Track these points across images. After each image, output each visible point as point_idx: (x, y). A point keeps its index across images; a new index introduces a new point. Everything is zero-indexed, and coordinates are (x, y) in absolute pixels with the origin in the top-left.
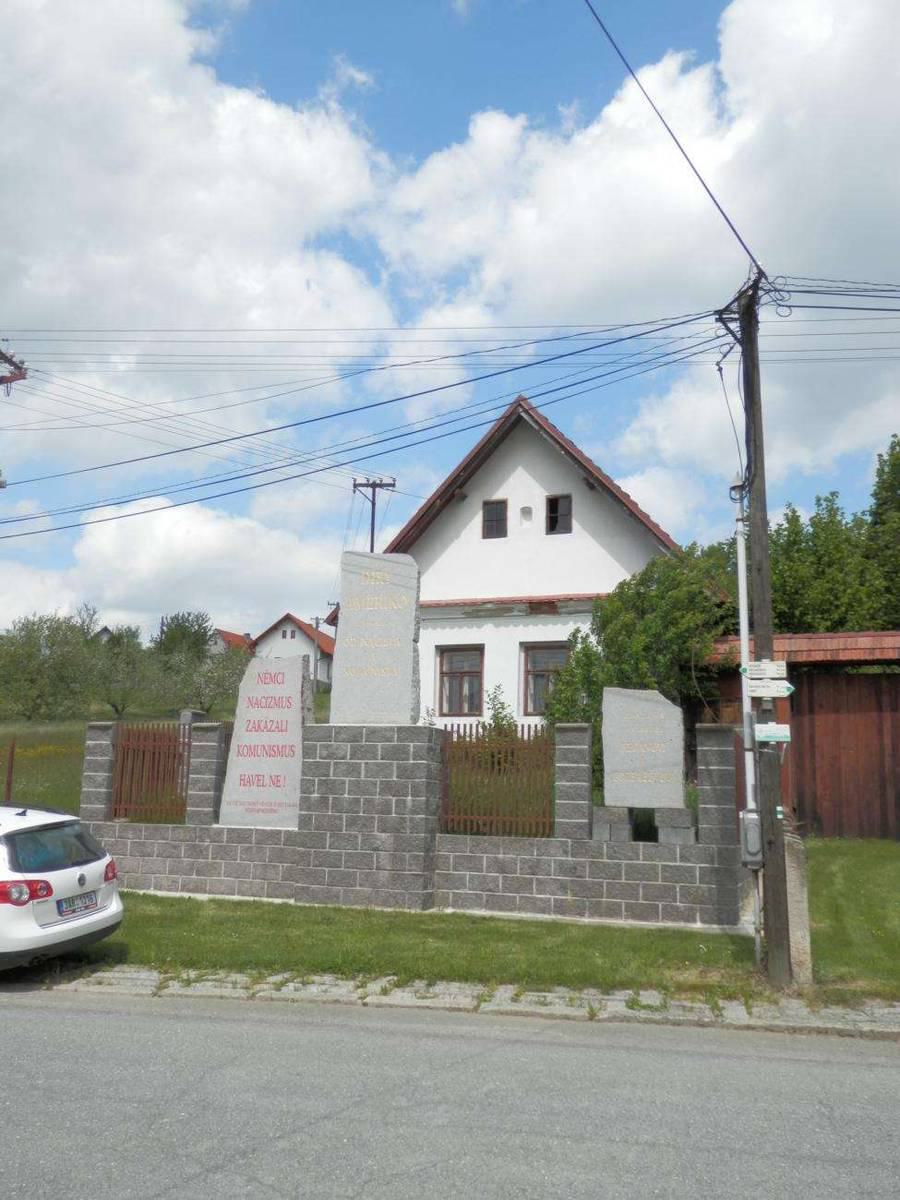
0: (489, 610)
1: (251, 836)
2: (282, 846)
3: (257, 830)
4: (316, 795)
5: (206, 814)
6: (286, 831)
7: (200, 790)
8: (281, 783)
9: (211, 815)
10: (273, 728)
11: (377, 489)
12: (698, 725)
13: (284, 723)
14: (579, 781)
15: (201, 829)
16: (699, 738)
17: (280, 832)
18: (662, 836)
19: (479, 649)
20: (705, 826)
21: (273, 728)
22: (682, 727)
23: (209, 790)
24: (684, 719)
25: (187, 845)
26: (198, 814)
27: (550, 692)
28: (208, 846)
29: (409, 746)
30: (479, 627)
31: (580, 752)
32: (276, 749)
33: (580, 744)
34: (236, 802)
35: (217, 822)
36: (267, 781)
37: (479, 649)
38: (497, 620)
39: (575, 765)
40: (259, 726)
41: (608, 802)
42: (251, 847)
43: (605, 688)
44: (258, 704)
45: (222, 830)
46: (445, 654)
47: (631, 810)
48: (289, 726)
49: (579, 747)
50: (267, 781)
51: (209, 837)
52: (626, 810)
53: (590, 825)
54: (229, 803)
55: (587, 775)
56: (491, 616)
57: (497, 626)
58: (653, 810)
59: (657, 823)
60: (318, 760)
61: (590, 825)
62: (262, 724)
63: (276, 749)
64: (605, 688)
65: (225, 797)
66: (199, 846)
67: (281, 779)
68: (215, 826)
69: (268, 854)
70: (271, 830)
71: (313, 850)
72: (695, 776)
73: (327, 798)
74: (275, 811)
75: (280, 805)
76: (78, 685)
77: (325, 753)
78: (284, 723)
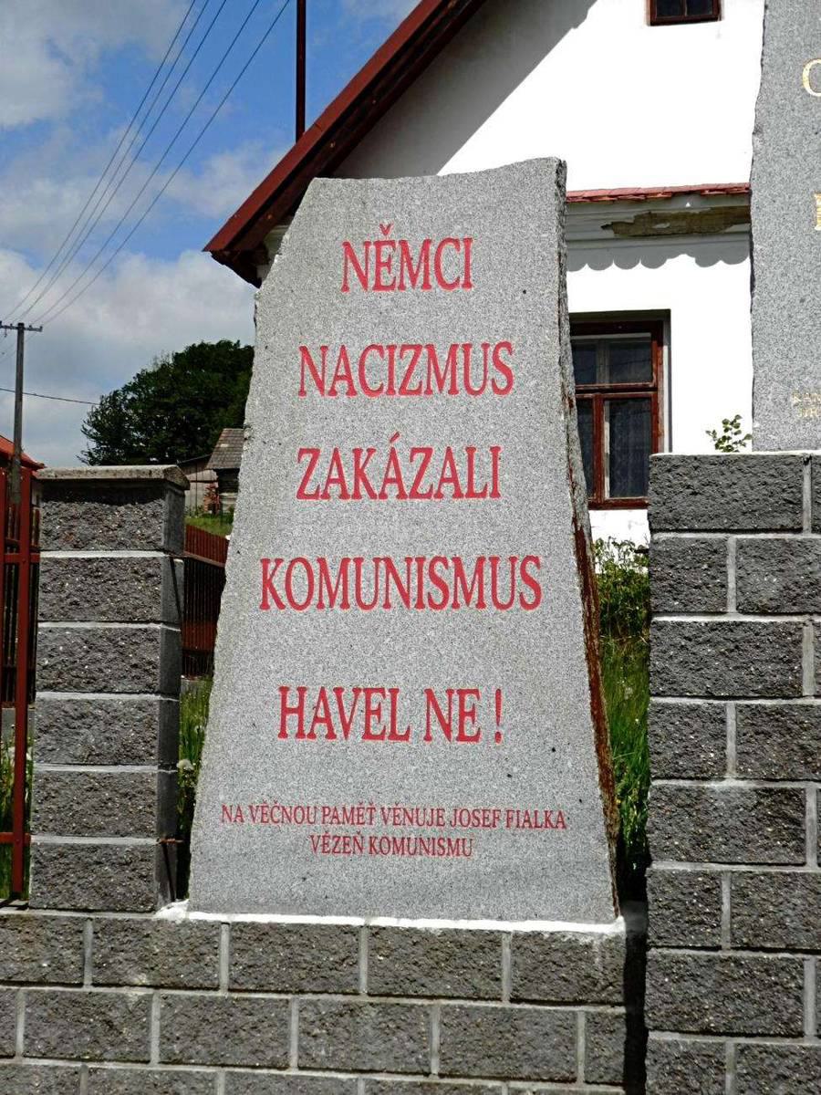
0: (685, 216)
1: (349, 960)
2: (506, 1004)
3: (377, 932)
4: (731, 782)
5: (126, 863)
6: (522, 942)
7: (92, 758)
8: (485, 719)
9: (151, 868)
10: (430, 480)
11: (16, 332)
13: (483, 457)
15: (104, 930)
17: (493, 940)
19: (654, 326)
21: (430, 480)
23: (137, 759)
25: (44, 1001)
26: (88, 860)
28: (145, 1004)
29: (717, 551)
30: (654, 263)
32: (448, 575)
34: (264, 812)
35: (179, 890)
36: (412, 714)
37: (654, 326)
38: (711, 244)
40: (359, 474)
42: (352, 1010)
44: (351, 379)
45: (208, 933)
46: (416, 388)
48: (505, 477)
50: (412, 714)
51: (145, 962)
54: (232, 814)
56: (689, 233)
57: (704, 261)
60: (732, 617)
62: (376, 469)
63: (448, 575)
65: (212, 794)
66: (101, 1008)
67: (485, 706)
68: (174, 912)
69: (436, 1040)
70: (445, 932)
71: (731, 1043)
73: (796, 798)
74: (455, 847)
75: (484, 820)
77: (769, 586)
78: (483, 457)
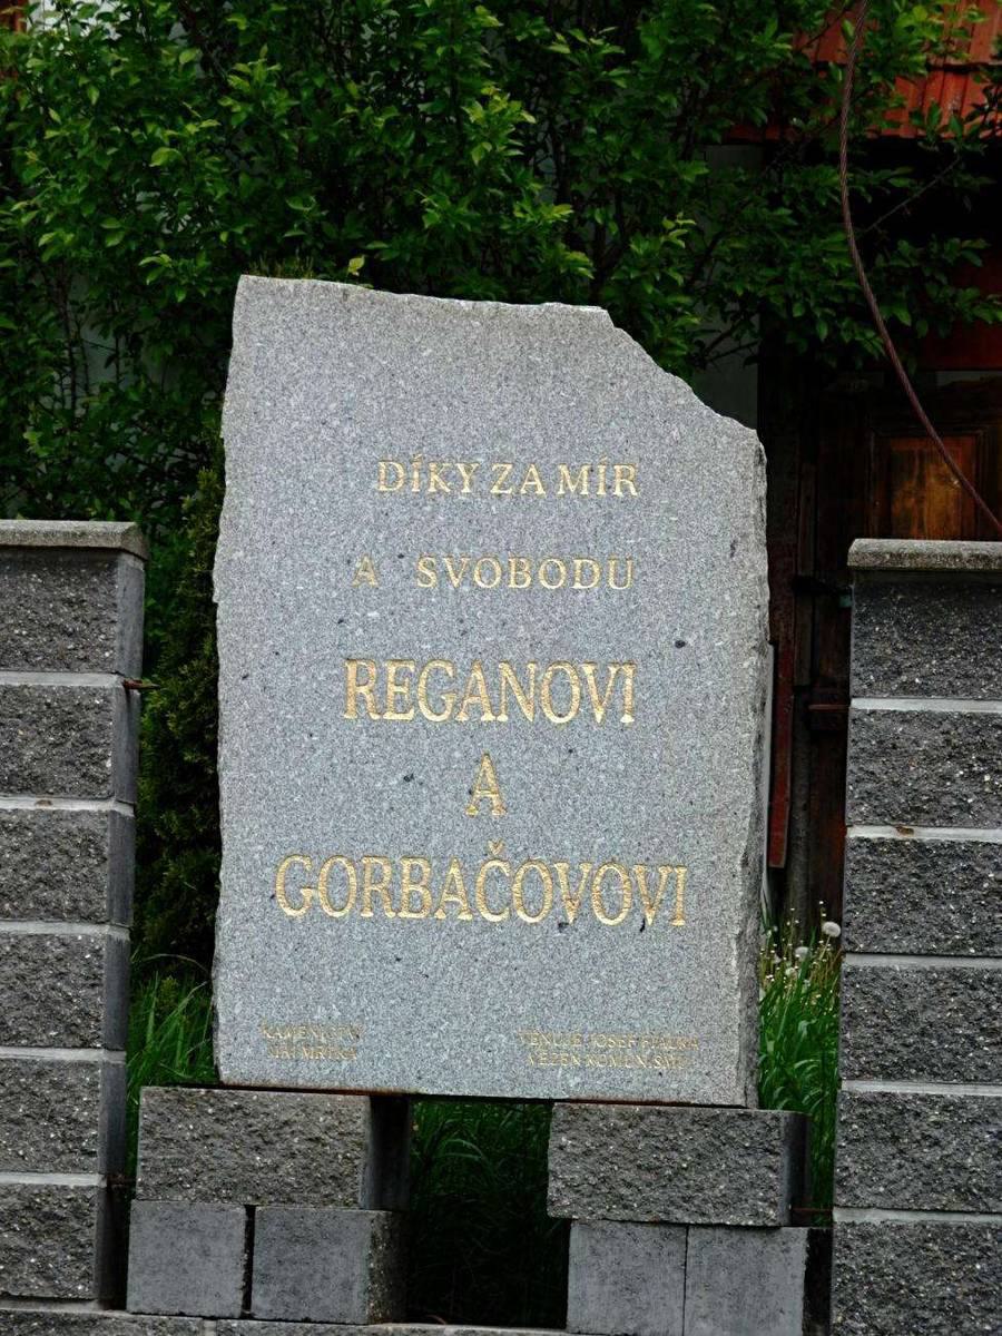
12: (864, 548)
14: (56, 914)
16: (871, 641)
18: (587, 1294)
20: (874, 1218)
22: (757, 561)
24: (773, 607)
27: (14, 264)
31: (66, 716)
33: (64, 662)
39: (27, 804)
41: (236, 1056)
43: (245, 282)
47: (390, 1109)
49: (55, 680)
52: (361, 1106)
53: (118, 1199)
55: (106, 877)
58: (539, 1111)
59: (561, 1199)
61: (118, 1199)
64: (245, 282)
72: (827, 894)
76: (661, 203)
